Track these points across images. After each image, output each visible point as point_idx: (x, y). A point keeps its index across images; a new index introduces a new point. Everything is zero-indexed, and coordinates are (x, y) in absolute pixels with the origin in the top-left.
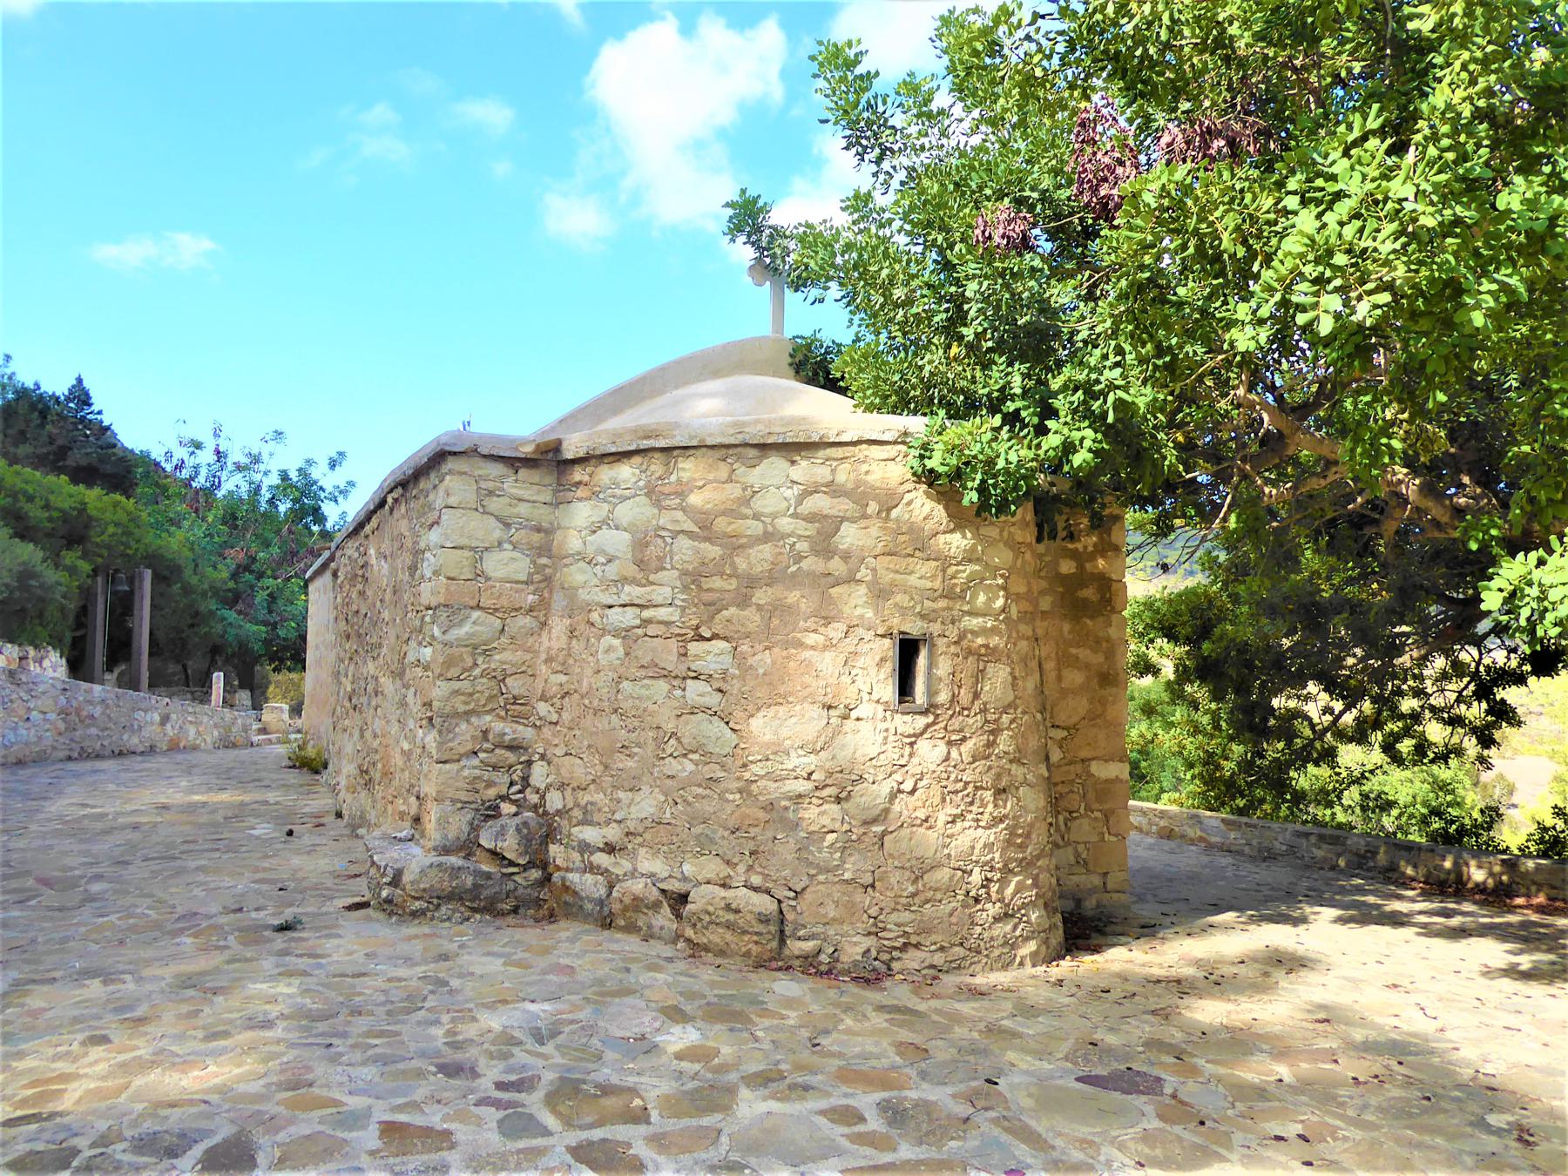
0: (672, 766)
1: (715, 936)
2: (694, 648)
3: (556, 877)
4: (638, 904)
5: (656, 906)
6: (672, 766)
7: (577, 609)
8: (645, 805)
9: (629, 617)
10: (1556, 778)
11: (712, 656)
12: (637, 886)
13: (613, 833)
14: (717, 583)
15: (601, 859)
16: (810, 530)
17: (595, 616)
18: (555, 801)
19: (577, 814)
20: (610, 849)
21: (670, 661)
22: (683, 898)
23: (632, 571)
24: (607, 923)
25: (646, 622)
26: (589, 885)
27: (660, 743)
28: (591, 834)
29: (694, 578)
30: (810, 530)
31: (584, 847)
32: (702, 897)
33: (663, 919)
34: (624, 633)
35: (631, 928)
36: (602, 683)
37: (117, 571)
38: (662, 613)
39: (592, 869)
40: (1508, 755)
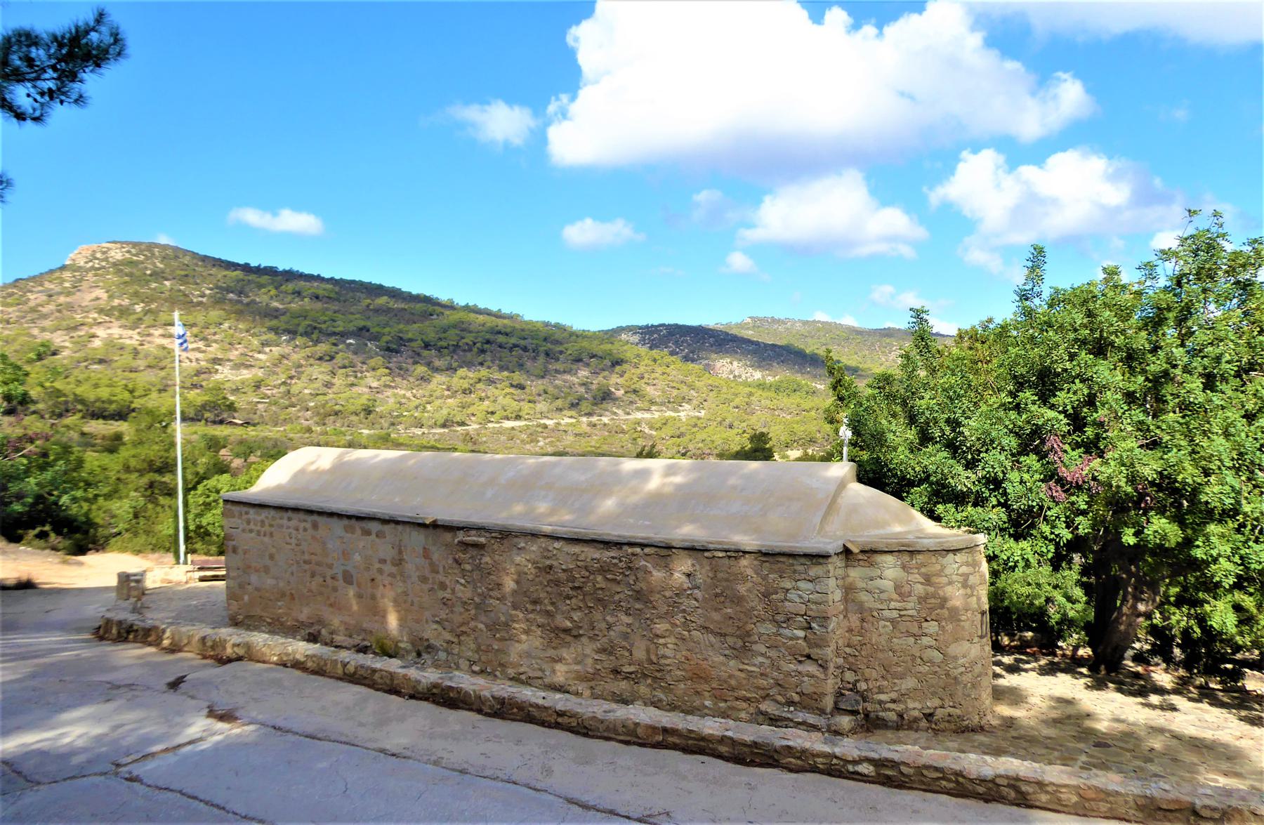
0: (921, 669)
1: (942, 726)
2: (925, 625)
3: (872, 715)
4: (916, 720)
5: (920, 720)
6: (921, 669)
7: (861, 608)
8: (909, 683)
9: (895, 614)
10: (81, 96)
11: (932, 627)
12: (916, 713)
13: (894, 695)
14: (933, 601)
15: (892, 706)
16: (961, 579)
17: (875, 614)
18: (862, 686)
19: (875, 690)
20: (894, 701)
21: (915, 630)
22: (931, 715)
23: (895, 596)
24: (898, 727)
25: (901, 616)
26: (892, 716)
27: (913, 660)
28: (883, 697)
29: (923, 599)
30: (961, 579)
31: (880, 702)
32: (940, 713)
33: (924, 724)
34: (892, 621)
35: (910, 728)
36: (883, 640)
37: (271, 535)
38: (910, 612)
39: (889, 710)
40: (750, 431)
